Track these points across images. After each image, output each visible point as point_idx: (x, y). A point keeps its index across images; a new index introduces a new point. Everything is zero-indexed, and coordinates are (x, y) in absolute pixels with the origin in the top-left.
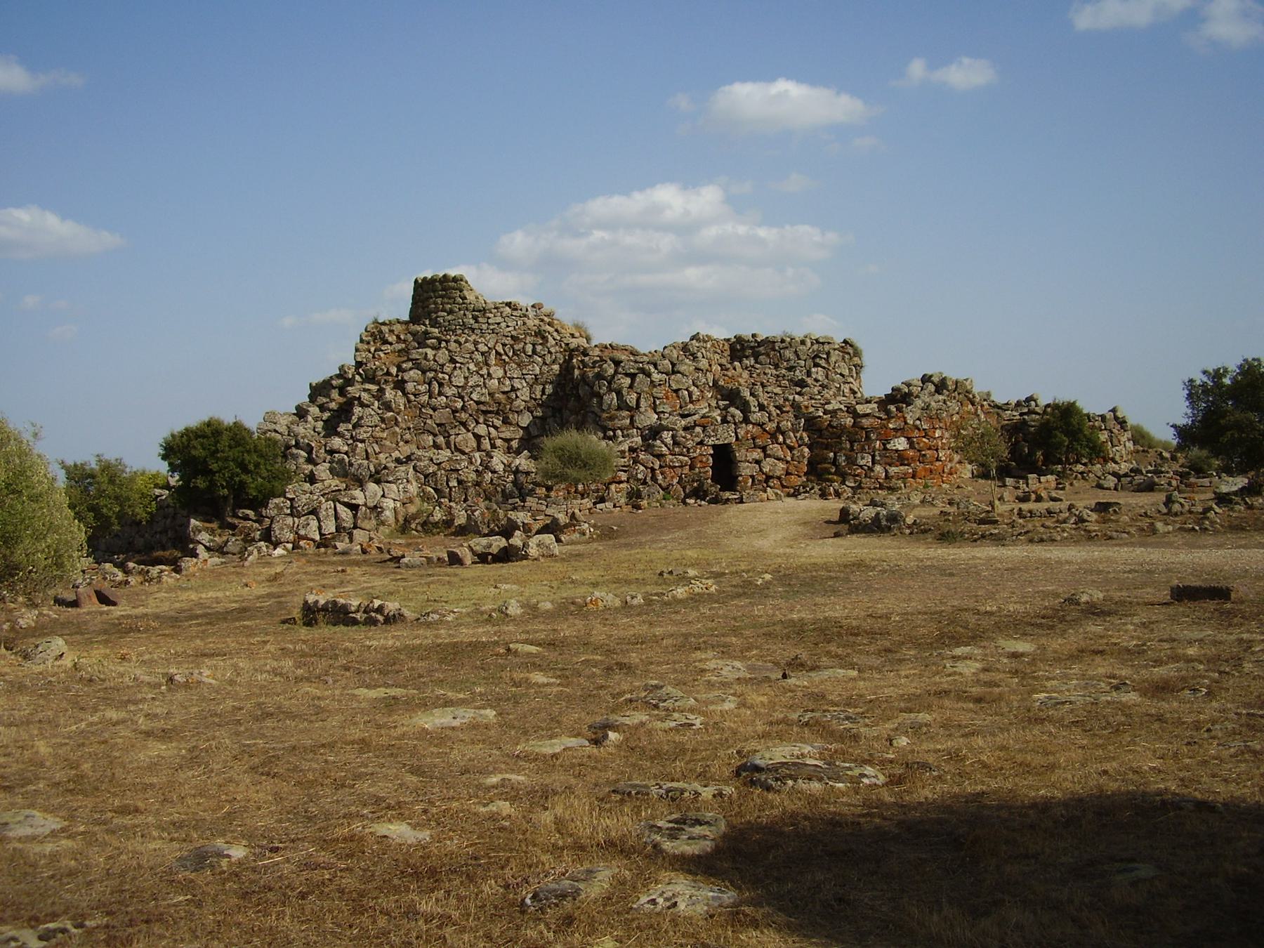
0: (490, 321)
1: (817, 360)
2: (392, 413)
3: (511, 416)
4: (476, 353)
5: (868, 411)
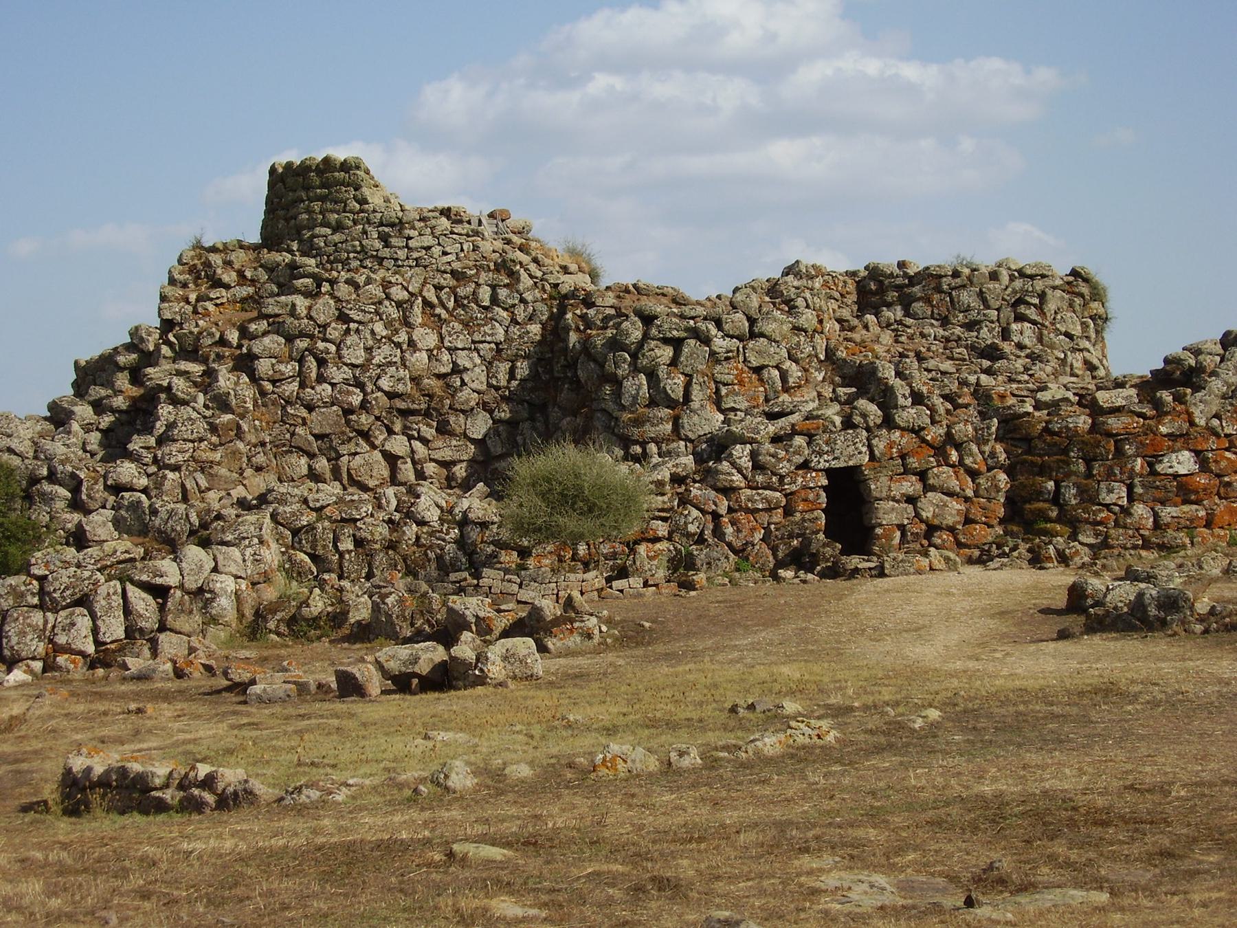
0: (412, 243)
1: (1022, 309)
2: (230, 416)
3: (452, 419)
4: (387, 303)
5: (1120, 402)
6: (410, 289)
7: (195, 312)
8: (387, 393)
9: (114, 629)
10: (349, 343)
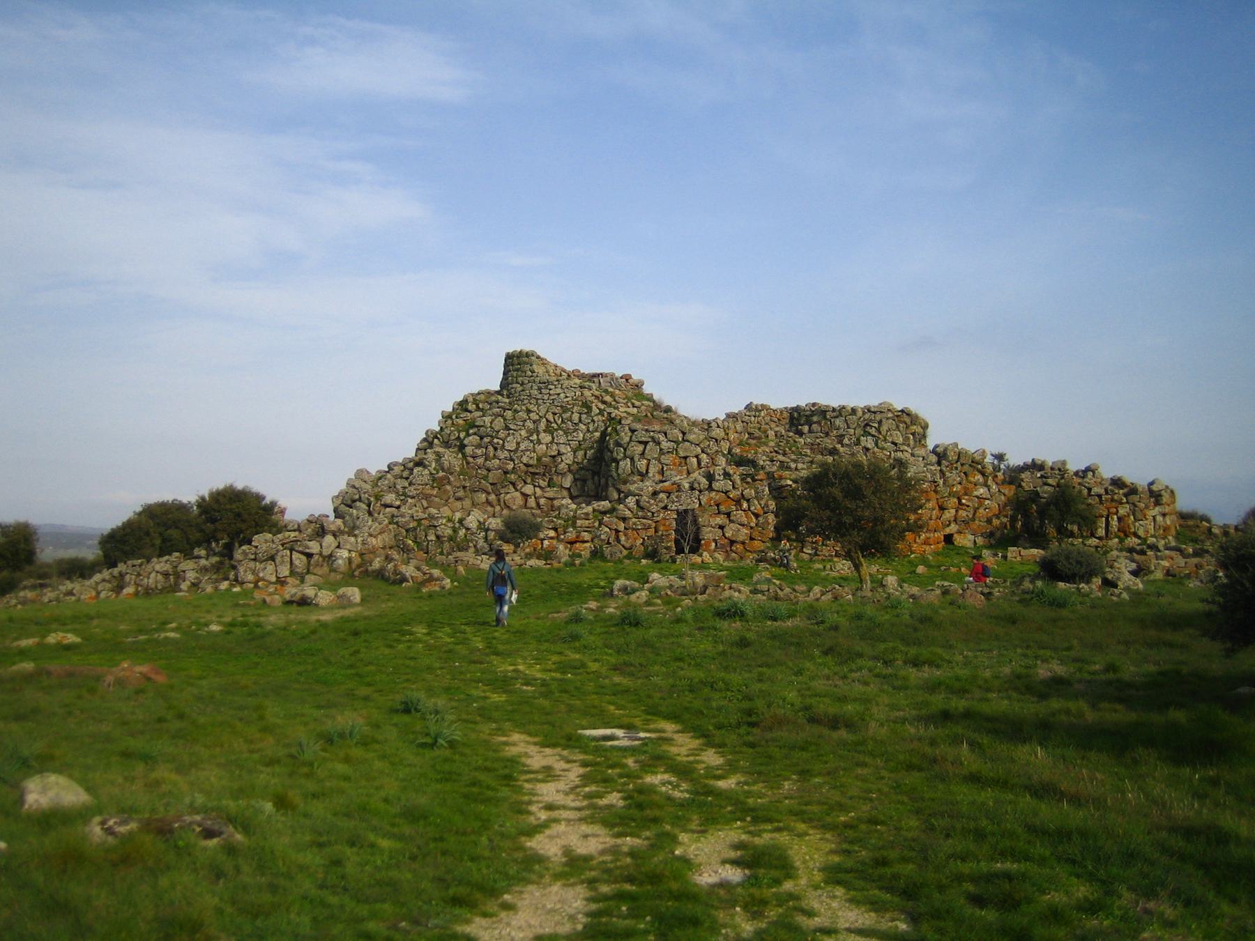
0: (551, 392)
3: (555, 478)
7: (453, 423)
8: (525, 464)
9: (285, 571)
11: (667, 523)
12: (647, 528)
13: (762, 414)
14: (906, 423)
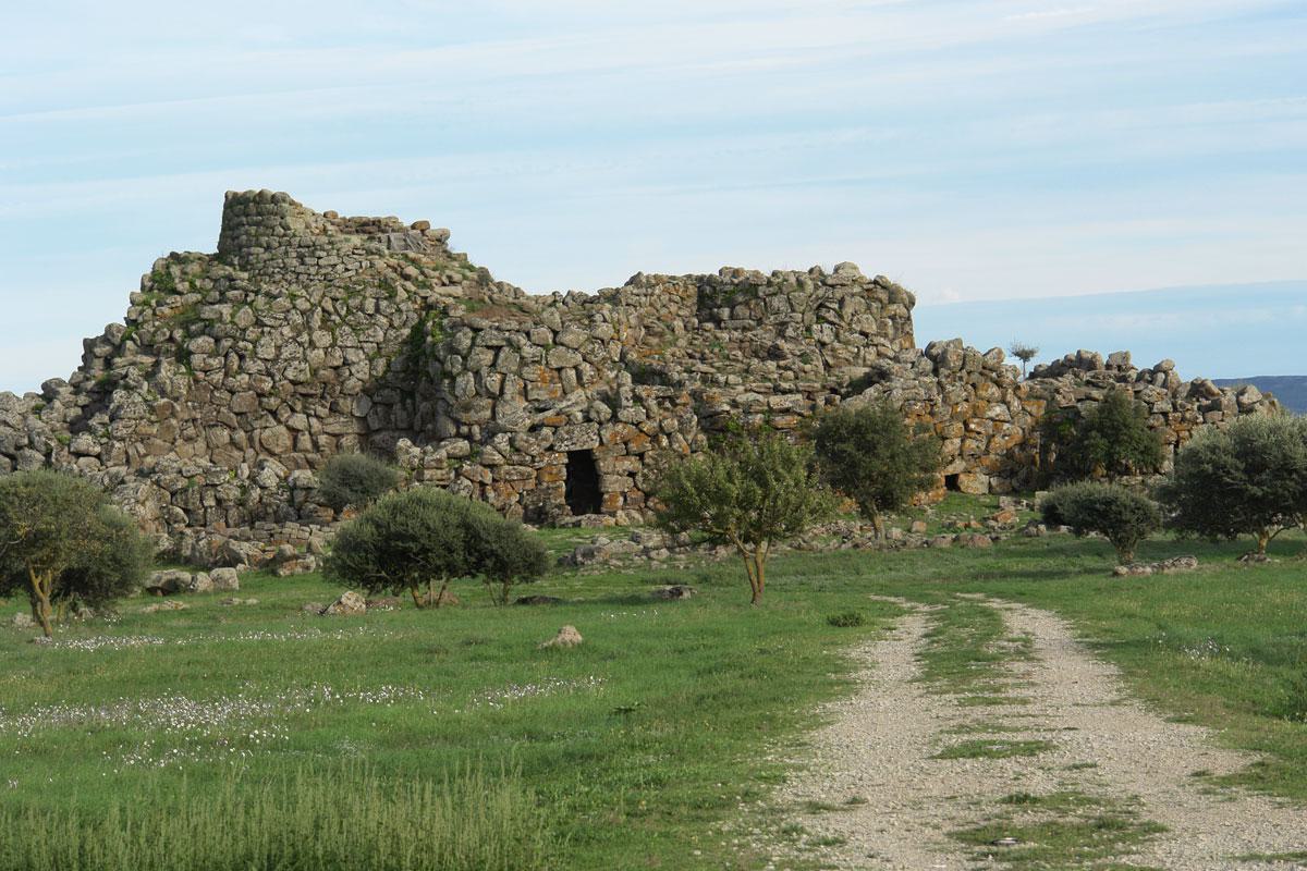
0: (321, 262)
1: (823, 312)
2: (166, 400)
3: (341, 401)
4: (293, 311)
5: (788, 405)
6: (312, 300)
7: (154, 314)
8: (292, 382)
10: (262, 342)
11: (555, 471)
12: (524, 478)
13: (657, 292)
14: (881, 301)
